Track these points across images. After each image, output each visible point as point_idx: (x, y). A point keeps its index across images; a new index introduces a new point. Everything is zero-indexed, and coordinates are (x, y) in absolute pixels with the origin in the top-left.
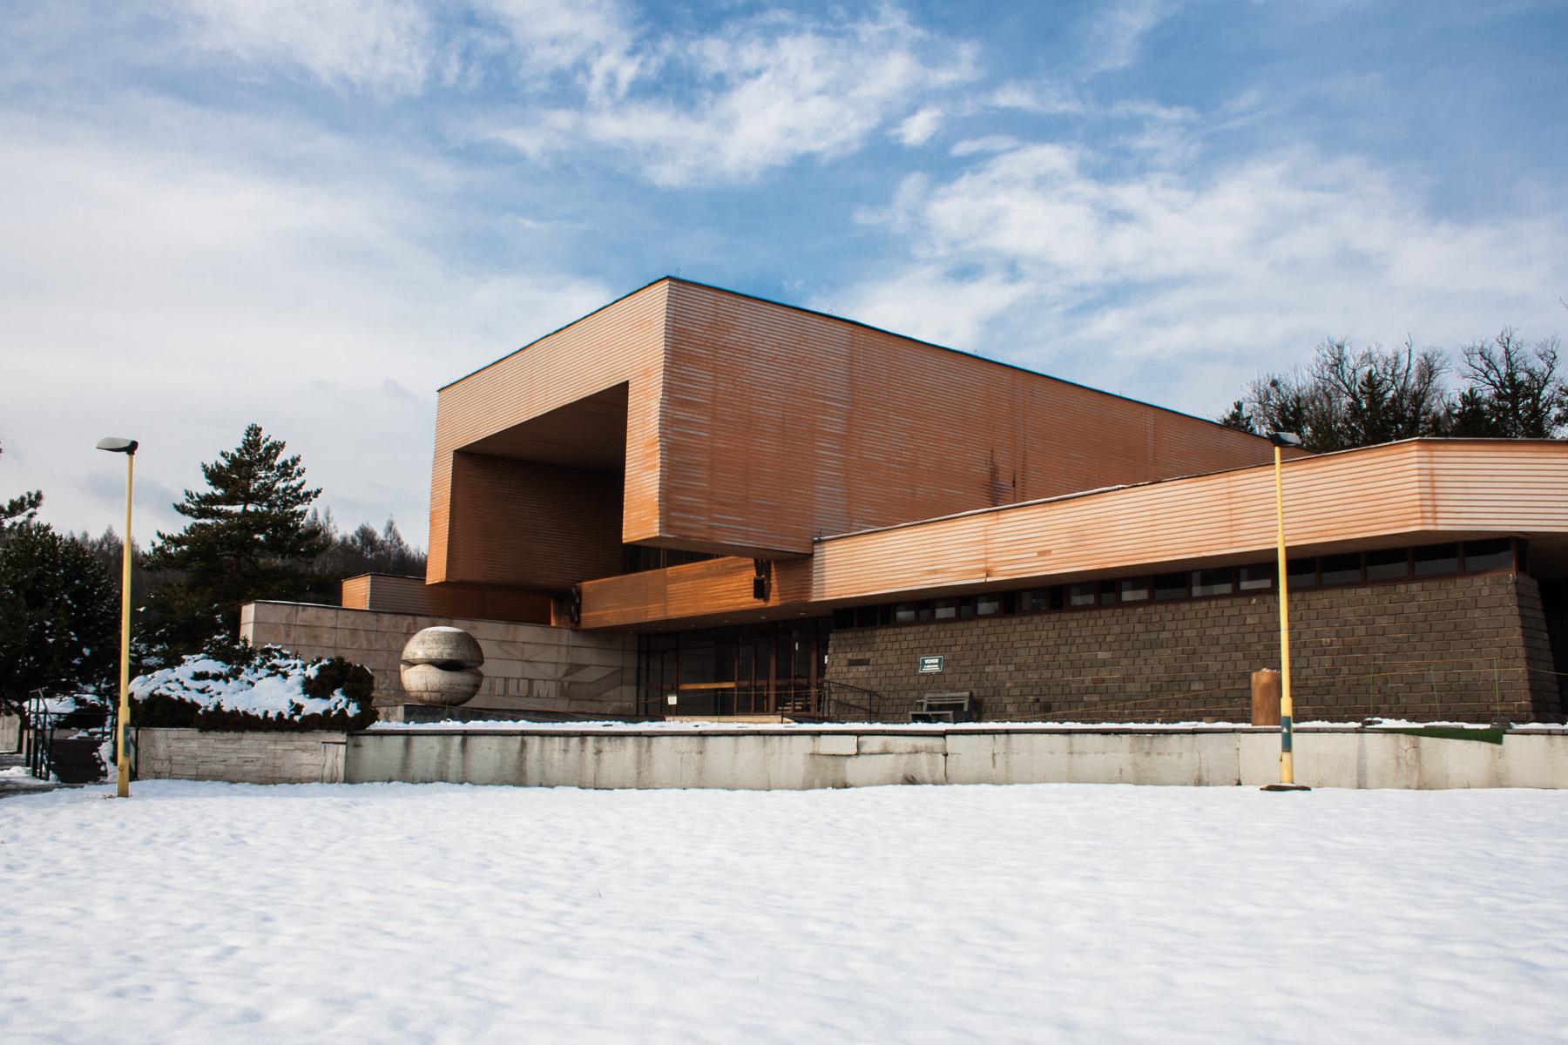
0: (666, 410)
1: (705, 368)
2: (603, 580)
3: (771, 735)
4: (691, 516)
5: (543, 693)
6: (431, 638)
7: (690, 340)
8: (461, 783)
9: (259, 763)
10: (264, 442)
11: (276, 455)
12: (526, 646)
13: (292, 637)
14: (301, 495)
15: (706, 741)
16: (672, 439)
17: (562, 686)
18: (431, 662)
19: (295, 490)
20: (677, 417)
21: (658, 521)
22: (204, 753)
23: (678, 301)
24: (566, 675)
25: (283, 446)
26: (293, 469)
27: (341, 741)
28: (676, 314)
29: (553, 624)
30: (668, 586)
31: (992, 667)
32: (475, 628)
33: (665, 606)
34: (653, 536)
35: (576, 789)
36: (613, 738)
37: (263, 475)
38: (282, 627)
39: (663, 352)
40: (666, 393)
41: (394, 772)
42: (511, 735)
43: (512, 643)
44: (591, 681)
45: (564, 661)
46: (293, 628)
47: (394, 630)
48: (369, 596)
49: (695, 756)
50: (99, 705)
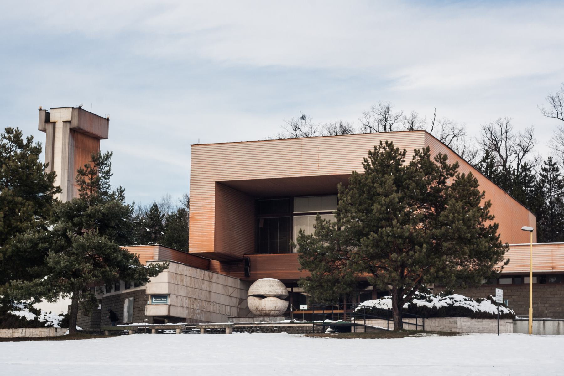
9: (488, 330)
22: (472, 326)
27: (510, 322)
31: (536, 305)
50: (64, 318)
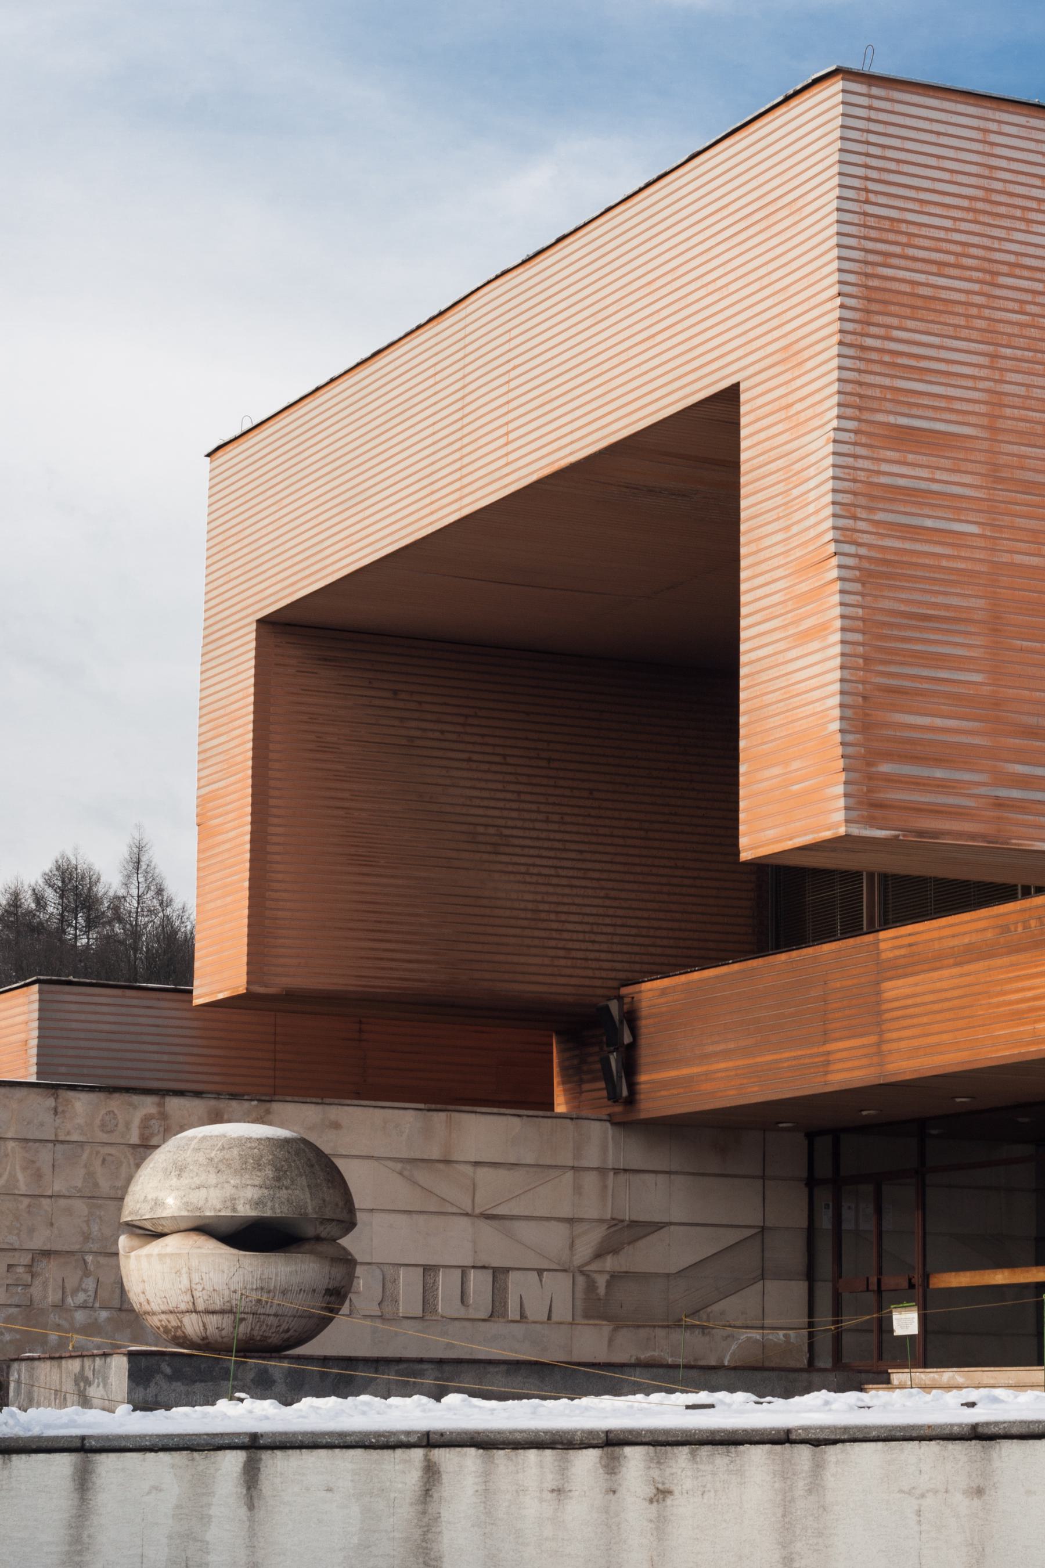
0: (850, 461)
1: (965, 333)
2: (696, 976)
4: (939, 773)
5: (536, 1311)
6: (201, 1158)
7: (911, 252)
12: (482, 1172)
15: (995, 1455)
16: (870, 546)
17: (591, 1286)
18: (205, 1229)
20: (883, 480)
21: (840, 789)
23: (873, 138)
24: (598, 1255)
28: (866, 178)
29: (560, 1107)
32: (336, 1126)
33: (879, 1044)
34: (827, 834)
36: (705, 1450)
39: (835, 290)
40: (849, 412)
43: (441, 1166)
44: (673, 1270)
45: (593, 1213)
47: (103, 1137)
48: (35, 1042)
49: (961, 1502)
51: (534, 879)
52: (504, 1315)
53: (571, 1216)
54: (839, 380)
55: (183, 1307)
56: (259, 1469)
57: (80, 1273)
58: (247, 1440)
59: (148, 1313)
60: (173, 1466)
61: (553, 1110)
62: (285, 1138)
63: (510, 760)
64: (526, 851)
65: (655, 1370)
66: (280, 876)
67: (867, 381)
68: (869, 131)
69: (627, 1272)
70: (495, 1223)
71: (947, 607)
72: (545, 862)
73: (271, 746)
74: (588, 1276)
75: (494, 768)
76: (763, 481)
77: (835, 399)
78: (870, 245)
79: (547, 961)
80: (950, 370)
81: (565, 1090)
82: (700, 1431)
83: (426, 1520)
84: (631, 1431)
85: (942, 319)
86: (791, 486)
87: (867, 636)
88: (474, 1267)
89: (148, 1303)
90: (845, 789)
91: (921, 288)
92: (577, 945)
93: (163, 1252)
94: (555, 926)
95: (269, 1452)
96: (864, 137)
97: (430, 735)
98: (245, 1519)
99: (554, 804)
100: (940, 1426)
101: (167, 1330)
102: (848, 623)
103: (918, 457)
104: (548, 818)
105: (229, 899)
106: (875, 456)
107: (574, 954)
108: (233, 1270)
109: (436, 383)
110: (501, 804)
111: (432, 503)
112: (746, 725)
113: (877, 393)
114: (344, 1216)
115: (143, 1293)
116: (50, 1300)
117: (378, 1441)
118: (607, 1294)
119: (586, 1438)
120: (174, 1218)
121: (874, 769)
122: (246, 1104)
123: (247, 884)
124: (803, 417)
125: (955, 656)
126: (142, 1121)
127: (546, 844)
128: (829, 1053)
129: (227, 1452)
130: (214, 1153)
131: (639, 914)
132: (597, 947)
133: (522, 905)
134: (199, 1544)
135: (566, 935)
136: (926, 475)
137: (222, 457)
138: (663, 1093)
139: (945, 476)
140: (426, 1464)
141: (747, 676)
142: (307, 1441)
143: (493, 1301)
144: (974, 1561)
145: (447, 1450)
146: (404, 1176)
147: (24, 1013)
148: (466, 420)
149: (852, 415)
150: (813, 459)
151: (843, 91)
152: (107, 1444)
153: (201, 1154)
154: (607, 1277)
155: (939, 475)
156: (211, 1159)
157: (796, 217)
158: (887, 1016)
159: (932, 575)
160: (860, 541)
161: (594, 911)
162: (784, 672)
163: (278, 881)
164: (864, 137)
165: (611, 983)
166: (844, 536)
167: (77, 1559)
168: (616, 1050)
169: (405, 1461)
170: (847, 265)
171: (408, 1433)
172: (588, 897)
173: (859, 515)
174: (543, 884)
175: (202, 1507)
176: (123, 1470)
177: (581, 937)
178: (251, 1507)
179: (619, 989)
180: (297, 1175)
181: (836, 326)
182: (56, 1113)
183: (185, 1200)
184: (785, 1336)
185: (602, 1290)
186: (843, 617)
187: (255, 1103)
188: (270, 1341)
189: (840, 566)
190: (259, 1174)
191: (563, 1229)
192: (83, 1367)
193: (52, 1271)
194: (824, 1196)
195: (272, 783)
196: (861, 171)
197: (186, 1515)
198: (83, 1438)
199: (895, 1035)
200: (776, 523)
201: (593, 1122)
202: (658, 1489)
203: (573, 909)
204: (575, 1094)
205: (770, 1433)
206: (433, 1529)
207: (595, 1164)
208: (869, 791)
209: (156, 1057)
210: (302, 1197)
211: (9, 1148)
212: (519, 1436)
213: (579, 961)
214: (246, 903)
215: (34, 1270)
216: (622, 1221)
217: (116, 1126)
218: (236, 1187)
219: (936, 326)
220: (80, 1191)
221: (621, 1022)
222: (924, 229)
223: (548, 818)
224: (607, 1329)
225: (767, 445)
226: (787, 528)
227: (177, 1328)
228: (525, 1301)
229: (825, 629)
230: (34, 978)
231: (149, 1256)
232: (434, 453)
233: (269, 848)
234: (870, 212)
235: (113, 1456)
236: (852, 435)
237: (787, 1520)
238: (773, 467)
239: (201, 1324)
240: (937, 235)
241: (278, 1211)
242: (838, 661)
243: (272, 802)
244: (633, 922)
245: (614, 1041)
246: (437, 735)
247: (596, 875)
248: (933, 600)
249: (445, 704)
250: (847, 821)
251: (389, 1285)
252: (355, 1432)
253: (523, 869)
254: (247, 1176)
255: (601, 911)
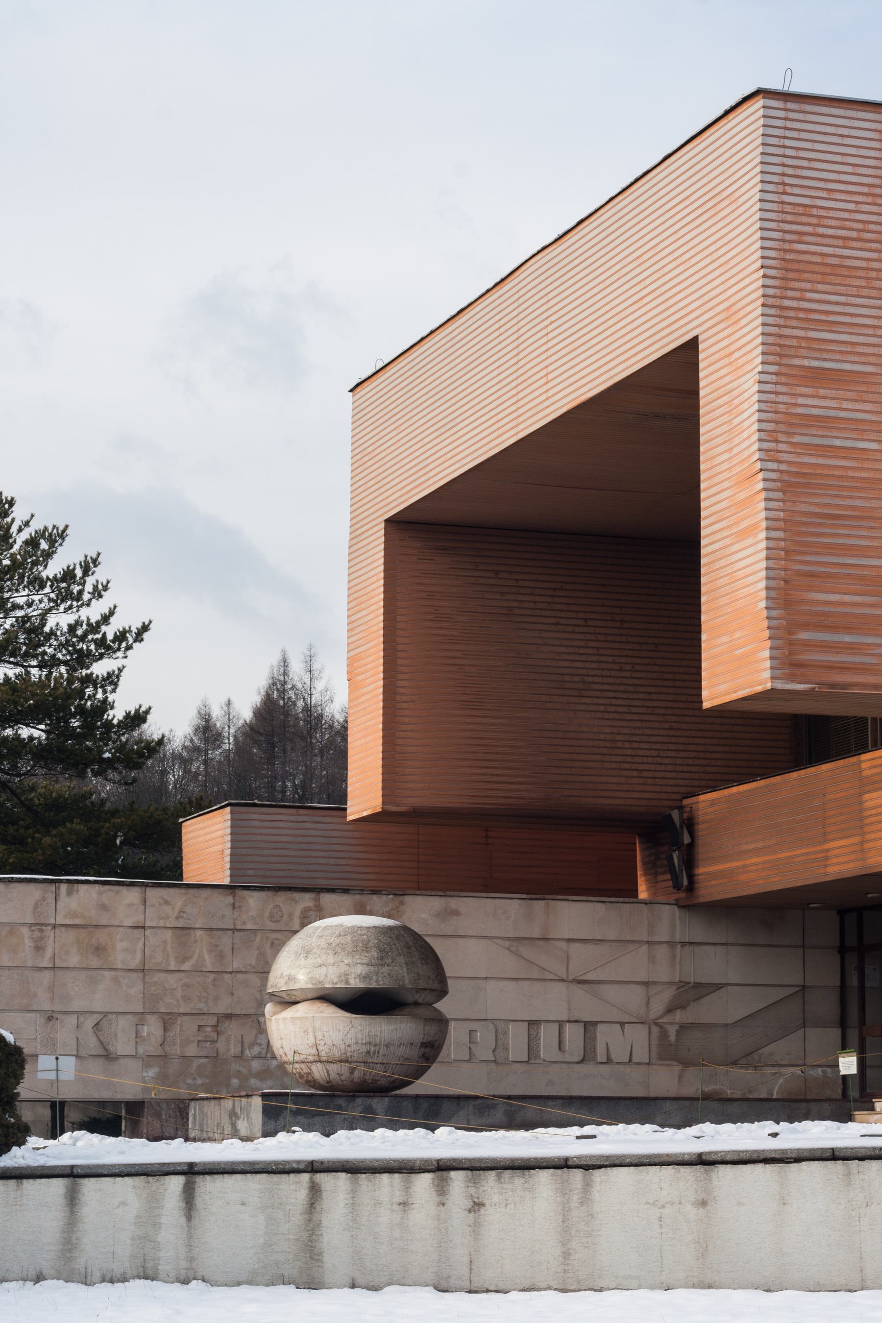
0: (772, 397)
1: (865, 292)
2: (734, 790)
3: (862, 1159)
4: (848, 638)
5: (620, 1054)
6: (323, 943)
7: (821, 230)
8: (186, 1282)
10: (20, 530)
11: (48, 555)
12: (574, 946)
13: (49, 952)
14: (110, 637)
15: (714, 1175)
16: (789, 463)
17: (664, 1035)
18: (327, 997)
19: (94, 628)
20: (800, 410)
21: (767, 653)
23: (788, 143)
24: (670, 1010)
25: (62, 535)
26: (83, 584)
28: (784, 175)
29: (643, 895)
30: (867, 796)
32: (456, 913)
33: (862, 843)
34: (759, 689)
35: (428, 1294)
36: (507, 1174)
37: (21, 601)
38: (25, 930)
39: (758, 264)
40: (771, 358)
41: (46, 1260)
42: (288, 1172)
43: (541, 943)
44: (730, 1021)
45: (664, 978)
46: (48, 931)
47: (273, 926)
48: (228, 852)
49: (692, 1212)
51: (611, 716)
52: (594, 1058)
53: (646, 980)
54: (763, 334)
55: (311, 1058)
56: (194, 1189)
57: (255, 1032)
58: (186, 1168)
59: (287, 1063)
60: (134, 1187)
61: (637, 896)
62: (389, 926)
63: (590, 623)
64: (605, 694)
65: (682, 1102)
66: (406, 720)
67: (785, 333)
68: (785, 138)
69: (692, 1023)
70: (585, 986)
71: (854, 508)
72: (620, 702)
73: (399, 618)
74: (661, 1027)
75: (577, 629)
76: (714, 413)
77: (760, 349)
78: (787, 227)
79: (623, 780)
80: (854, 322)
81: (646, 880)
82: (505, 1159)
83: (311, 1225)
84: (454, 1160)
85: (847, 282)
86: (733, 416)
87: (787, 533)
88: (569, 1021)
89: (286, 1055)
90: (770, 653)
91: (829, 258)
92: (646, 767)
93: (295, 1016)
94: (629, 752)
95: (201, 1176)
96: (781, 142)
97: (526, 605)
98: (185, 1225)
99: (627, 656)
100: (676, 1155)
101: (301, 1076)
102: (772, 524)
103: (828, 391)
104: (621, 667)
105: (369, 738)
106: (793, 392)
107: (645, 774)
108: (347, 1029)
109: (500, 335)
110: (583, 658)
111: (498, 429)
112: (707, 602)
113: (794, 342)
114: (436, 986)
115: (282, 1047)
116: (232, 1052)
117: (277, 1168)
118: (677, 1040)
119: (423, 1165)
120: (302, 990)
121: (794, 637)
122: (384, 898)
123: (381, 726)
124: (741, 362)
125: (858, 546)
126: (302, 912)
127: (621, 688)
128: (827, 850)
129: (172, 1176)
130: (333, 939)
131: (697, 741)
132: (663, 768)
133: (602, 737)
134: (153, 1244)
135: (637, 760)
136: (835, 405)
137: (361, 392)
138: (714, 883)
139: (850, 406)
140: (311, 1184)
141: (706, 565)
142: (227, 1168)
143: (584, 1047)
144: (700, 1255)
145: (326, 1174)
146: (512, 952)
147: (220, 829)
148: (520, 364)
149: (775, 361)
150: (746, 395)
151: (764, 107)
152: (89, 1171)
153: (323, 940)
154: (677, 1027)
155: (845, 405)
156: (330, 944)
157: (733, 207)
158: (867, 821)
159: (841, 483)
160: (781, 459)
161: (660, 739)
162: (729, 562)
163: (405, 724)
164: (781, 142)
165: (674, 796)
166: (768, 456)
167: (68, 1255)
168: (678, 849)
169: (297, 1183)
170: (768, 244)
171: (298, 1162)
172: (655, 728)
173: (780, 439)
174: (618, 720)
175: (154, 1217)
176: (100, 1190)
177: (650, 760)
178: (189, 1218)
179: (681, 800)
180: (396, 955)
181: (760, 292)
182: (234, 907)
183: (310, 975)
184: (823, 1071)
185: (673, 1038)
186: (767, 519)
187: (391, 896)
188: (379, 1083)
189: (764, 480)
190: (367, 955)
191: (640, 990)
192: (234, 1105)
193: (233, 1030)
194: (852, 960)
195: (399, 647)
196: (779, 169)
197: (144, 1223)
198: (72, 1167)
199: (873, 836)
200: (723, 446)
201: (663, 905)
202: (474, 1202)
203: (643, 738)
204: (653, 884)
205: (554, 1161)
206: (316, 1233)
207: (666, 939)
208: (791, 654)
209: (324, 861)
210: (400, 972)
211: (198, 935)
212: (376, 1164)
213: (649, 780)
214: (381, 741)
215: (219, 1029)
216: (688, 983)
217: (282, 916)
218: (348, 965)
219: (842, 288)
220: (254, 967)
221: (681, 827)
222: (831, 212)
223: (621, 667)
224: (677, 1068)
225: (717, 384)
226: (731, 449)
227: (309, 1074)
228: (609, 1046)
229: (756, 529)
230: (227, 802)
231: (285, 1019)
232: (499, 390)
233: (398, 698)
234: (787, 201)
235: (93, 1180)
236: (774, 377)
237: (566, 1225)
238: (720, 402)
239: (325, 1071)
240: (842, 216)
241: (381, 983)
242: (764, 554)
243: (399, 662)
244: (693, 747)
245: (677, 843)
246: (532, 605)
247: (662, 711)
248: (842, 503)
249: (537, 580)
250: (772, 678)
251: (501, 1036)
252: (262, 1162)
253: (602, 708)
254: (357, 957)
255: (666, 739)
